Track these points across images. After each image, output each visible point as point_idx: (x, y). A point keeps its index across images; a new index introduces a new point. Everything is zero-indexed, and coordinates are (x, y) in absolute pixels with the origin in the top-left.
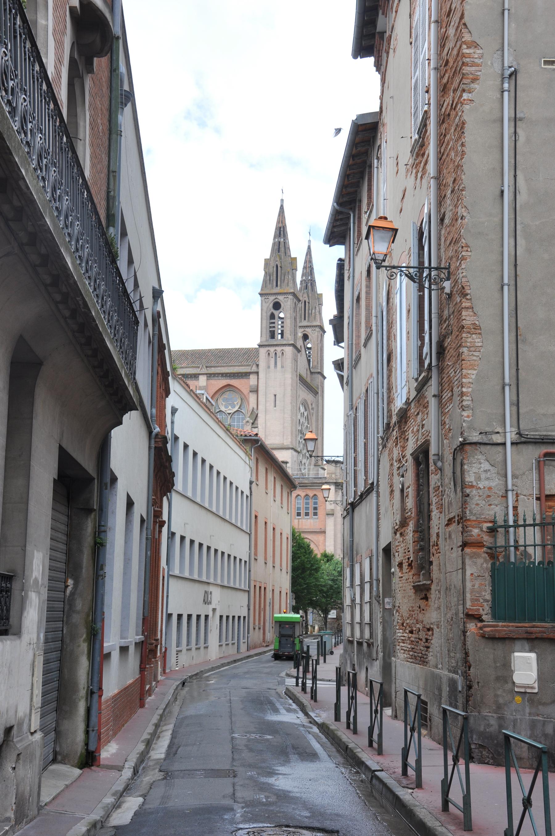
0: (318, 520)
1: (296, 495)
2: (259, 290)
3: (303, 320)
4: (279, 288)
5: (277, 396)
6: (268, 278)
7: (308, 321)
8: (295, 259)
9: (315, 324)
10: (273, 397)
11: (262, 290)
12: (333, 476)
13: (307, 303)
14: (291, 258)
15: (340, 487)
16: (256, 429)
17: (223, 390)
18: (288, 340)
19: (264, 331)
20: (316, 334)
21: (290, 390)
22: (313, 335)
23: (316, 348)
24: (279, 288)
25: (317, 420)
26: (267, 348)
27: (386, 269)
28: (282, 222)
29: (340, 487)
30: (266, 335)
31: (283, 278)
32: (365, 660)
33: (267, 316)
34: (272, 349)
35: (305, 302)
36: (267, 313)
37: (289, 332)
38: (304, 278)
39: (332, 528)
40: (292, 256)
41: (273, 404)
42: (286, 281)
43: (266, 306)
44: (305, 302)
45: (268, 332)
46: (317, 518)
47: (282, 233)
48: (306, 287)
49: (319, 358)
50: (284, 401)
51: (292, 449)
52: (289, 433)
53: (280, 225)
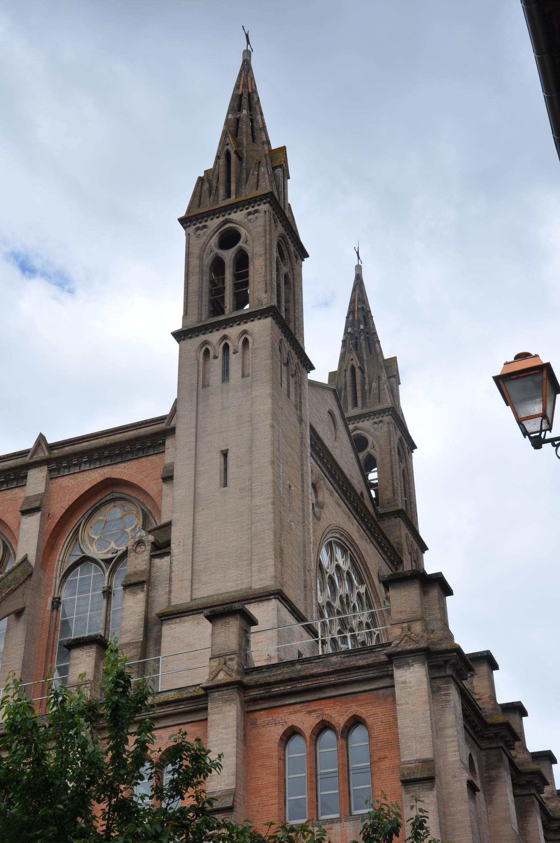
1: (280, 730)
5: (230, 455)
9: (378, 407)
10: (218, 459)
11: (188, 211)
13: (358, 371)
14: (271, 151)
17: (95, 501)
19: (194, 299)
20: (385, 428)
21: (268, 428)
23: (387, 460)
24: (233, 196)
27: (554, 445)
28: (245, 85)
29: (449, 672)
30: (200, 308)
31: (244, 176)
33: (201, 266)
34: (214, 337)
35: (353, 369)
36: (201, 258)
37: (261, 286)
41: (217, 479)
42: (252, 180)
43: (197, 243)
44: (353, 369)
47: (245, 102)
48: (356, 346)
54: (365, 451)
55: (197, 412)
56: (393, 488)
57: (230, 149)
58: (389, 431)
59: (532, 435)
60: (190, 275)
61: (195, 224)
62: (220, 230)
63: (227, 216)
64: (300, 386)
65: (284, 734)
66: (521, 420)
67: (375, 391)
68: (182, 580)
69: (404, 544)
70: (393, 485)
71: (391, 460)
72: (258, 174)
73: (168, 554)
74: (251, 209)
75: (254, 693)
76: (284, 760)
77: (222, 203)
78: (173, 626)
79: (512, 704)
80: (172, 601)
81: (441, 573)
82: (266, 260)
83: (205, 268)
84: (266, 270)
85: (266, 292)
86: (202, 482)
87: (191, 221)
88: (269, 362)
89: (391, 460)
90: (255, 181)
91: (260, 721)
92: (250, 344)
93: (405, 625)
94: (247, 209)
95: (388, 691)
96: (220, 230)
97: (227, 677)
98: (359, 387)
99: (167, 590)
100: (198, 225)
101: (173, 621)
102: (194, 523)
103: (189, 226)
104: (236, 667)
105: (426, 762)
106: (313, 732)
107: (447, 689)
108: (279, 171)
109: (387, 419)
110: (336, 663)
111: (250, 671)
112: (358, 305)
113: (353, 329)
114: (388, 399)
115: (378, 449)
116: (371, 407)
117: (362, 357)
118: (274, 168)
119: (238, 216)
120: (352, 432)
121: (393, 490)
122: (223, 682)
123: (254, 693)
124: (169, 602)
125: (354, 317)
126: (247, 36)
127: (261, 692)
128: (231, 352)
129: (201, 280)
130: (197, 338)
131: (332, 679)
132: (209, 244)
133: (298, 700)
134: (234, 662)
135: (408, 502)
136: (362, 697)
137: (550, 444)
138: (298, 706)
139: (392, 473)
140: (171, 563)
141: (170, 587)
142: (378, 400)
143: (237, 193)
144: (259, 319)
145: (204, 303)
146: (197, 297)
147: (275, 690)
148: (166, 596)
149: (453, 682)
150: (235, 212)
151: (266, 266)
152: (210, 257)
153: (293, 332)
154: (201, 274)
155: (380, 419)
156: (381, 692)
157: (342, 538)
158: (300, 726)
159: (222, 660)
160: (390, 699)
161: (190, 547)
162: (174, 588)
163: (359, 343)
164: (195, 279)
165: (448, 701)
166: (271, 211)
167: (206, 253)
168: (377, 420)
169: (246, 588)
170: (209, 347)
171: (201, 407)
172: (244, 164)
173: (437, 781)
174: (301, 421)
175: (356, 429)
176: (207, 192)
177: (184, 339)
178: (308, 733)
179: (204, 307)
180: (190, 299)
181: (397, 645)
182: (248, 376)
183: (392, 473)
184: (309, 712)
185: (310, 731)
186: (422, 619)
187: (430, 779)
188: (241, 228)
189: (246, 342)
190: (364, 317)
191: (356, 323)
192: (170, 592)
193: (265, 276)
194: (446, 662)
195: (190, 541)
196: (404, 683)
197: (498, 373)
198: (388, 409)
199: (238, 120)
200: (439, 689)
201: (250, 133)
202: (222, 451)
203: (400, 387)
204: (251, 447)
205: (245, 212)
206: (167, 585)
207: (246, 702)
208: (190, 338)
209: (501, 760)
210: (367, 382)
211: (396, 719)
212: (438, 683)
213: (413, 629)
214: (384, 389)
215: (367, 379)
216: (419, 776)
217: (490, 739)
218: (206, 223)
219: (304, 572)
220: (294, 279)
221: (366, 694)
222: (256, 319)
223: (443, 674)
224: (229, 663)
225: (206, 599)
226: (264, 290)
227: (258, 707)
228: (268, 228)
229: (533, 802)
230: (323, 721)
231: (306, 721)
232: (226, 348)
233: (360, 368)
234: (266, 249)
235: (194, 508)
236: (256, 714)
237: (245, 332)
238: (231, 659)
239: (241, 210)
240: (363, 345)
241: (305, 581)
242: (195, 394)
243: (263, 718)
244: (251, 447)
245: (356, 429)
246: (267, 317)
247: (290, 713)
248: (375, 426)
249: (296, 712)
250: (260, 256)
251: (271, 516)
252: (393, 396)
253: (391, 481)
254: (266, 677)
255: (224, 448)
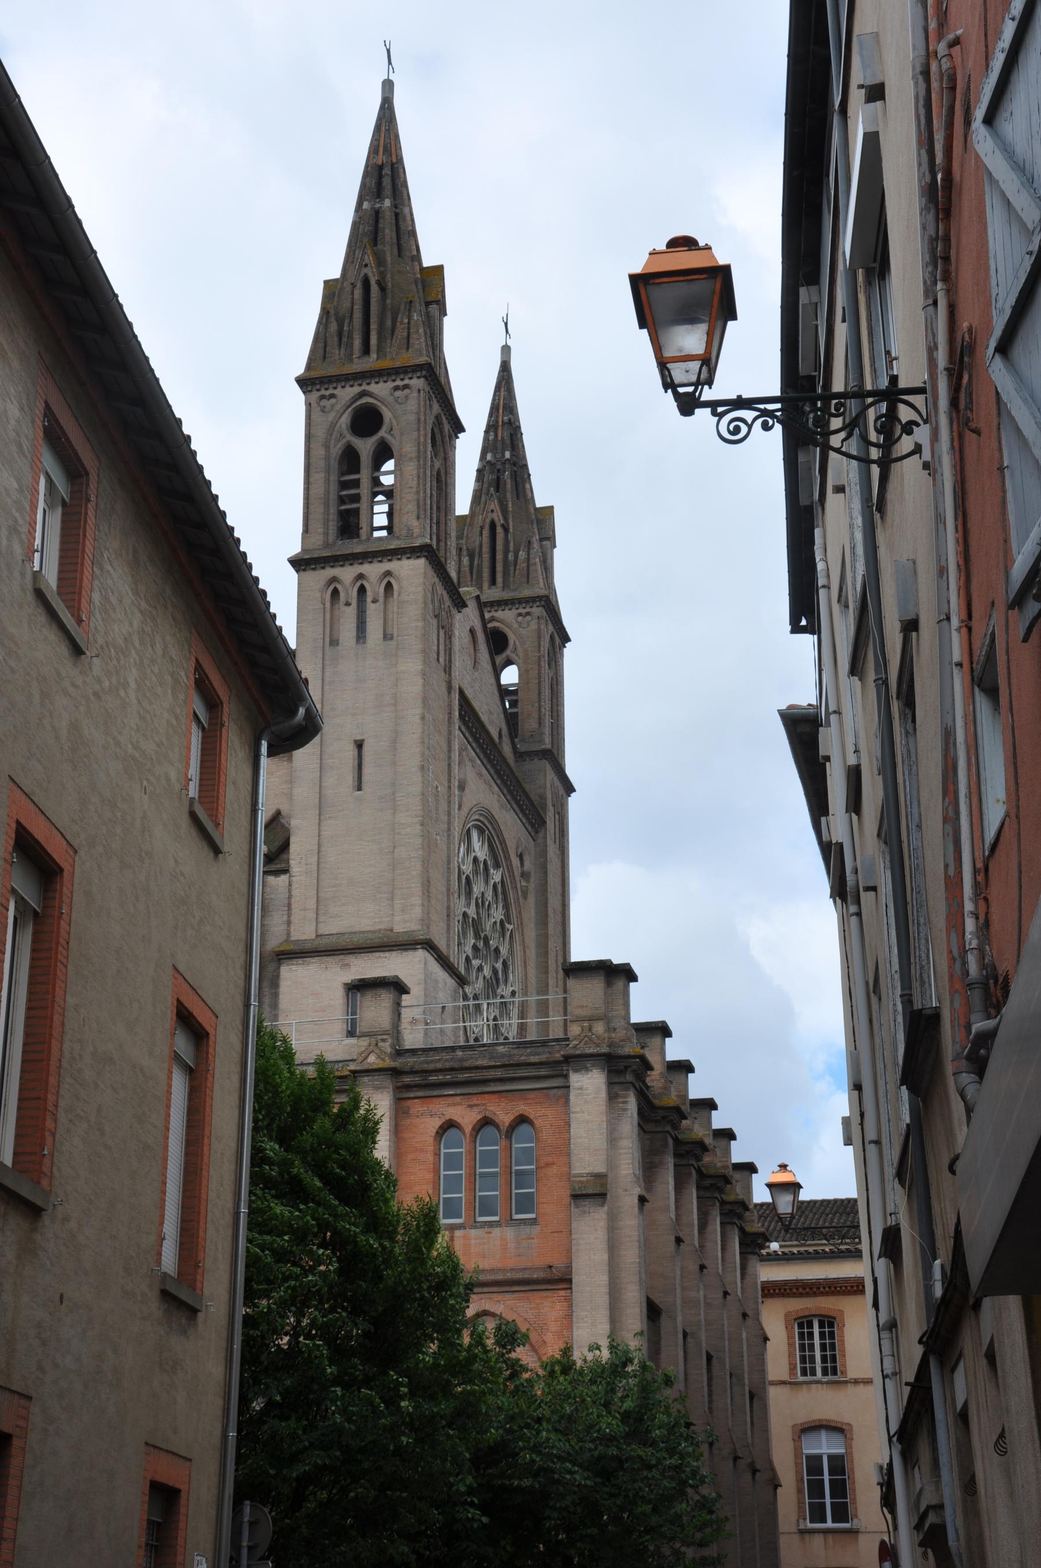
0: (536, 1229)
1: (437, 1123)
2: (300, 369)
3: (486, 585)
4: (374, 356)
5: (366, 748)
6: (333, 327)
7: (506, 586)
8: (438, 271)
9: (526, 593)
10: (351, 752)
11: (309, 367)
12: (599, 1028)
13: (499, 530)
14: (423, 269)
15: (629, 1077)
16: (284, 878)
18: (410, 535)
19: (318, 509)
20: (534, 626)
21: (417, 719)
22: (524, 632)
24: (374, 356)
25: (543, 920)
26: (330, 572)
27: (714, 413)
28: (387, 150)
29: (629, 1077)
30: (326, 526)
31: (389, 323)
32: (387, 1166)
33: (327, 458)
34: (347, 574)
35: (493, 526)
36: (327, 446)
37: (412, 507)
38: (489, 457)
39: (601, 1256)
40: (426, 264)
41: (350, 779)
42: (401, 333)
44: (493, 526)
45: (333, 516)
46: (534, 1222)
47: (387, 182)
48: (498, 484)
49: (547, 705)
50: (394, 764)
51: (429, 945)
52: (416, 887)
53: (380, 159)
54: (504, 655)
55: (323, 680)
56: (540, 715)
57: (370, 274)
58: (539, 630)
59: (681, 390)
60: (312, 470)
61: (318, 390)
62: (354, 406)
63: (365, 387)
64: (450, 638)
65: (441, 1127)
66: (665, 361)
67: (522, 565)
68: (305, 909)
69: (549, 796)
70: (540, 710)
71: (539, 674)
72: (409, 323)
73: (286, 871)
74: (399, 383)
75: (407, 1079)
76: (440, 1155)
77: (359, 365)
78: (294, 968)
79: (679, 1062)
80: (292, 934)
81: (628, 964)
82: (418, 468)
83: (332, 461)
84: (418, 484)
85: (418, 518)
86: (329, 781)
87: (313, 384)
88: (420, 624)
89: (539, 674)
90: (405, 334)
91: (412, 1111)
92: (396, 593)
93: (586, 1024)
94: (394, 381)
95: (560, 1092)
96: (354, 406)
97: (378, 1061)
98: (499, 557)
99: (285, 918)
100: (323, 392)
101: (295, 961)
102: (319, 836)
103: (310, 391)
104: (389, 1050)
105: (599, 1176)
106: (473, 1129)
107: (626, 1097)
108: (434, 308)
109: (537, 611)
110: (503, 1056)
111: (399, 1053)
112: (503, 416)
113: (494, 455)
114: (541, 580)
115: (521, 654)
116: (515, 590)
117: (507, 506)
118: (428, 304)
119: (381, 389)
120: (490, 622)
121: (540, 718)
122: (375, 1067)
123: (407, 1079)
124: (288, 935)
125: (496, 436)
126: (388, 51)
127: (417, 1079)
128: (369, 599)
129: (327, 480)
130: (322, 571)
131: (499, 1073)
132: (338, 425)
133: (458, 1091)
134: (387, 1044)
135: (555, 725)
136: (532, 1095)
137: (709, 410)
138: (458, 1099)
139: (539, 694)
140: (290, 885)
141: (289, 915)
142: (525, 580)
143: (380, 349)
144: (409, 558)
145: (331, 517)
146: (322, 506)
147: (433, 1078)
148: (284, 927)
149: (632, 1089)
150: (377, 383)
151: (419, 477)
152: (339, 445)
153: (443, 560)
154: (328, 471)
155: (528, 610)
156: (553, 1092)
157: (486, 822)
158: (459, 1120)
159: (373, 1041)
160: (562, 1101)
161: (314, 867)
162: (295, 918)
163: (501, 481)
164: (318, 477)
165: (625, 1110)
166: (427, 388)
167: (333, 437)
168: (523, 611)
169: (386, 930)
170: (339, 587)
171: (327, 674)
172: (388, 301)
173: (609, 1196)
174: (450, 689)
175: (493, 619)
176: (336, 339)
177: (304, 570)
178: (468, 1129)
179: (331, 523)
180: (311, 507)
181: (575, 1046)
182: (392, 639)
183: (539, 694)
184: (471, 1106)
185: (470, 1128)
186: (605, 1018)
187: (603, 1196)
188: (383, 407)
189: (389, 586)
190: (511, 435)
191: (499, 446)
192: (289, 923)
193: (418, 492)
194: (626, 1068)
195: (315, 859)
196: (581, 1089)
197: (638, 269)
198: (540, 598)
199: (377, 214)
200: (617, 1096)
201: (395, 241)
202: (356, 741)
203: (555, 550)
204: (394, 741)
205: (390, 385)
206: (285, 913)
207: (397, 1088)
208: (314, 569)
209: (665, 1145)
210: (511, 549)
211: (568, 1124)
212: (616, 1088)
213: (594, 1030)
214: (535, 564)
215: (512, 544)
216: (591, 1192)
217: (657, 1122)
218: (335, 392)
219: (448, 896)
220: (446, 474)
221: (536, 1092)
222: (404, 557)
223: (622, 1080)
224: (381, 1044)
225: (335, 937)
226: (415, 514)
227: (412, 1095)
228: (422, 418)
229: (691, 1173)
230: (485, 1118)
231: (467, 1116)
232: (362, 590)
233: (503, 526)
234: (419, 451)
235: (320, 815)
236: (409, 1103)
237: (388, 573)
238: (383, 1040)
239: (385, 382)
240: (509, 486)
241: (448, 907)
242: (320, 655)
243: (417, 1107)
244: (394, 741)
245: (493, 619)
246: (418, 557)
247: (449, 1105)
248: (520, 618)
249: (454, 1105)
250: (411, 459)
251: (419, 840)
252: (546, 569)
253: (536, 705)
254: (422, 1063)
255: (359, 738)
